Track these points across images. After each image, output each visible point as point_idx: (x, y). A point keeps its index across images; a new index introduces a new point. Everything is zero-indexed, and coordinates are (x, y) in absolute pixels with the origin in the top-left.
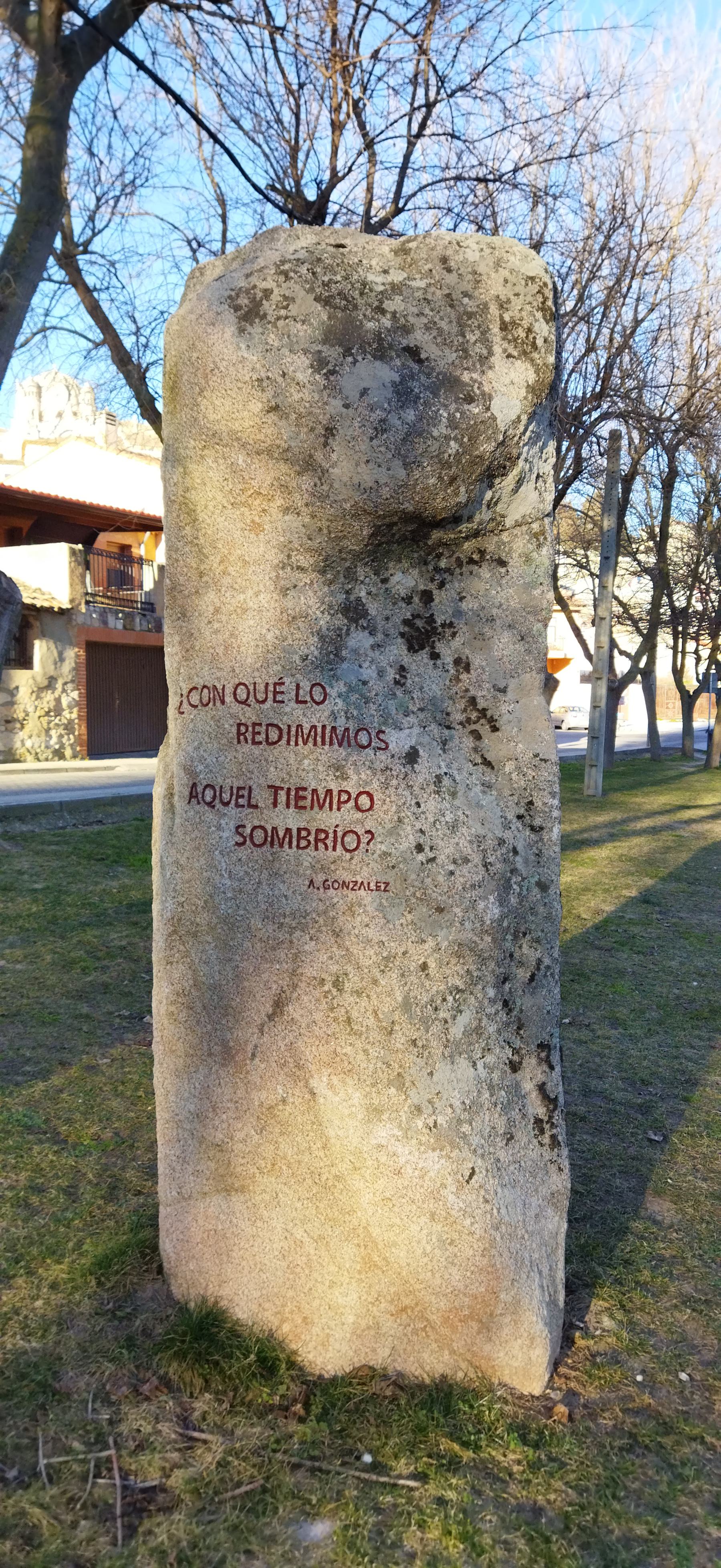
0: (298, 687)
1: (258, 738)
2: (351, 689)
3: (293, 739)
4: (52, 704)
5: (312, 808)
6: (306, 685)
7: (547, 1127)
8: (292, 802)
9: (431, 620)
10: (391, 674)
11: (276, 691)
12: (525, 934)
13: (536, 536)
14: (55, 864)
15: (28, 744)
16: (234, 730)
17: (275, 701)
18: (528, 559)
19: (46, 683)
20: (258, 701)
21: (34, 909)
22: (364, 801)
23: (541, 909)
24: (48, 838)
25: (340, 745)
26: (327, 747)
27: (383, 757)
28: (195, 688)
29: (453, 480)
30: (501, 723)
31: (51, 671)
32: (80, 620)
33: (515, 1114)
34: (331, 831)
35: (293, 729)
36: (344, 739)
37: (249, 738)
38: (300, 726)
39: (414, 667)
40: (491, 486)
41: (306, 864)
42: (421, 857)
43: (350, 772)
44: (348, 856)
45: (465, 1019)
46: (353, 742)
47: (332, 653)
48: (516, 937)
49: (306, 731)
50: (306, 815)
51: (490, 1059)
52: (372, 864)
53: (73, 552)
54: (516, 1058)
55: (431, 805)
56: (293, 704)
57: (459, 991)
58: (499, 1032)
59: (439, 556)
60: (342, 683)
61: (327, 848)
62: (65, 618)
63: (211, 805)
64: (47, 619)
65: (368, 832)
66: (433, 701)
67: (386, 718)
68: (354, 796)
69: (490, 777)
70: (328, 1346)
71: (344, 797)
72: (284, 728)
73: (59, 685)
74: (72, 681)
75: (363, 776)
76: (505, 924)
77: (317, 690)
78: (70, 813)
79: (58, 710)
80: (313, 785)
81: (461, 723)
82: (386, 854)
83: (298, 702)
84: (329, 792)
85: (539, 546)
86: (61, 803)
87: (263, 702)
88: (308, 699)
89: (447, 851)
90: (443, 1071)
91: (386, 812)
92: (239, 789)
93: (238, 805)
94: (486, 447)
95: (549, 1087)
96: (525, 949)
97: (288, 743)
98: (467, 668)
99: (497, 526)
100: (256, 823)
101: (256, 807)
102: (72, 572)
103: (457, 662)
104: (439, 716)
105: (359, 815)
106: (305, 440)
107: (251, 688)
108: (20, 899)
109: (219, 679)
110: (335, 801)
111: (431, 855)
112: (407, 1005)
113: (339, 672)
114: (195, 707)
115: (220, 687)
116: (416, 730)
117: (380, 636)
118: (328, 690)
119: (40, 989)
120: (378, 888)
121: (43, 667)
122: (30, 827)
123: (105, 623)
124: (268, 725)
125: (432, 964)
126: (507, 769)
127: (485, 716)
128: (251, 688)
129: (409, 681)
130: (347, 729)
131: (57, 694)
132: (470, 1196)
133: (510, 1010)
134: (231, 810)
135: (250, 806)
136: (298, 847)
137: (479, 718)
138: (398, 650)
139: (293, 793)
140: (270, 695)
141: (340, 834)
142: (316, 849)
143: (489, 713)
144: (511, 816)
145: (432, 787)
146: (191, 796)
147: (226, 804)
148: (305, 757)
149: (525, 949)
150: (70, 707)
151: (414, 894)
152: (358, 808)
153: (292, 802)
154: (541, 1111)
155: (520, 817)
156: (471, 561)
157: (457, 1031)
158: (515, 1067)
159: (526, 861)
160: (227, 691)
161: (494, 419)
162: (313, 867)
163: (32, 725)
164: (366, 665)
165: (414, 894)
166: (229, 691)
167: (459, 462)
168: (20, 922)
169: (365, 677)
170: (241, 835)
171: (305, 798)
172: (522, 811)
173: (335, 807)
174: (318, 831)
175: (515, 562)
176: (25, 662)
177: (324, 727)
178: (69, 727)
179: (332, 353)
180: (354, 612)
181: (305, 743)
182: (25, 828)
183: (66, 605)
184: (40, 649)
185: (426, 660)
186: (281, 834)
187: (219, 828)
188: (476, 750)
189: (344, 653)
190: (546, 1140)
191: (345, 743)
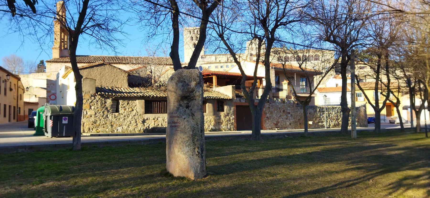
15: (223, 127)
31: (228, 112)
32: (235, 101)
36: (178, 117)
47: (178, 109)
53: (233, 87)
55: (186, 123)
70: (176, 174)
73: (230, 115)
79: (230, 120)
90: (185, 148)
94: (190, 90)
99: (195, 96)
102: (233, 91)
106: (175, 90)
112: (182, 142)
123: (241, 101)
132: (187, 159)
138: (185, 109)
150: (232, 119)
157: (187, 144)
158: (194, 149)
163: (224, 123)
176: (223, 110)
178: (232, 124)
179: (177, 83)
180: (180, 105)
184: (226, 108)
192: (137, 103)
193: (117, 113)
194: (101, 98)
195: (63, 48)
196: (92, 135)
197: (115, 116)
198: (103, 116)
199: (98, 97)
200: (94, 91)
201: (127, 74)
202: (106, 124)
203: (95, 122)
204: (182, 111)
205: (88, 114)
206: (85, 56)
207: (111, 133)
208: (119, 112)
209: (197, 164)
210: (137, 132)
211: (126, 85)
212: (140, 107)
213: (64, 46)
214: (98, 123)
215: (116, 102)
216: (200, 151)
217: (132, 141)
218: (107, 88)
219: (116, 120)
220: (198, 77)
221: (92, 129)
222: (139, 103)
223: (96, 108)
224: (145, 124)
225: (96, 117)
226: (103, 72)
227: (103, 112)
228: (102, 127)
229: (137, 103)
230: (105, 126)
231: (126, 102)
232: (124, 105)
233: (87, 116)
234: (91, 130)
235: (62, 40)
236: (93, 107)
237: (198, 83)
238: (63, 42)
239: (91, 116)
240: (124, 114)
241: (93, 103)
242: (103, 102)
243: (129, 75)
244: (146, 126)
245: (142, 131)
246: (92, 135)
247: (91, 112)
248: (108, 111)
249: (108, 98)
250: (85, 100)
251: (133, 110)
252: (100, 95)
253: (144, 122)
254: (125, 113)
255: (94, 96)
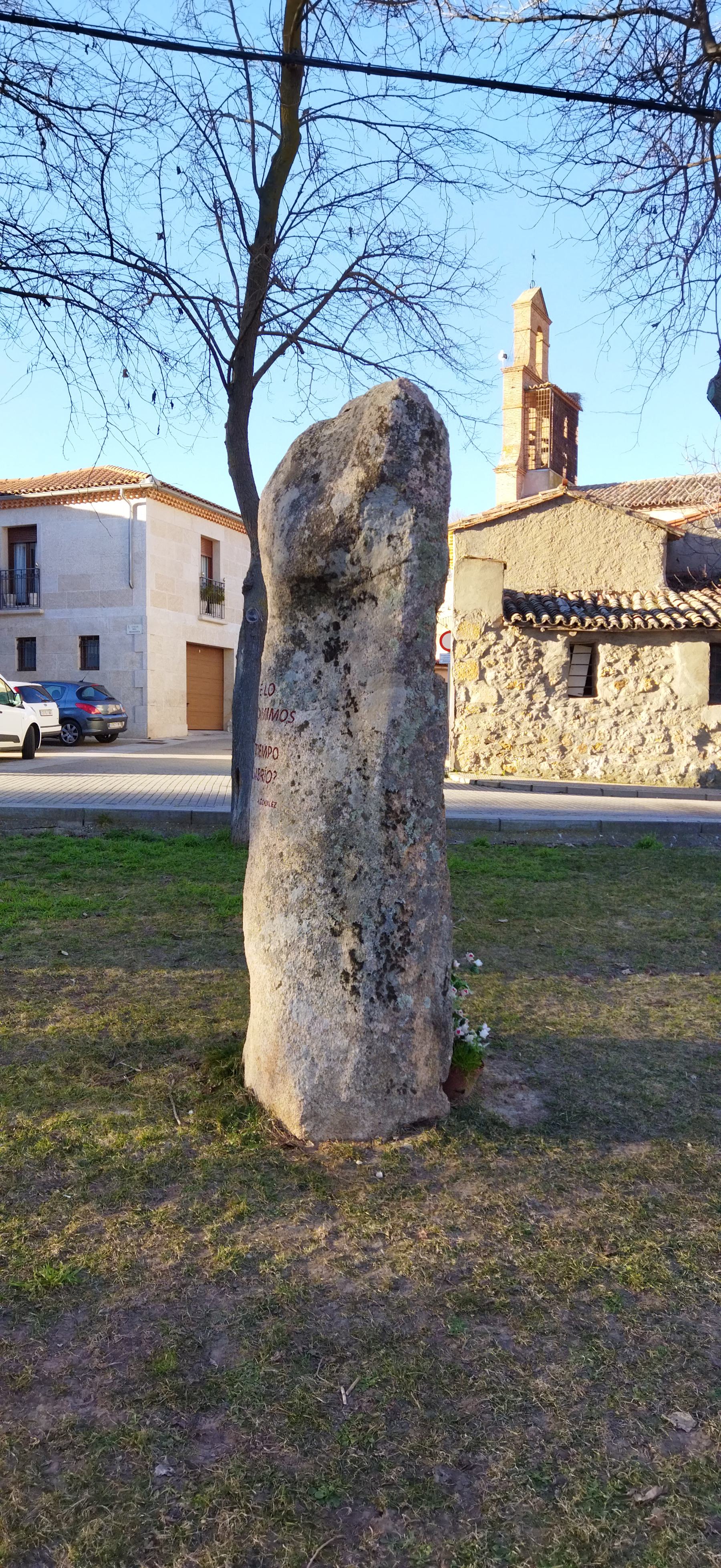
7: (351, 979)
9: (338, 639)
10: (313, 676)
12: (351, 847)
13: (394, 577)
18: (388, 594)
23: (363, 833)
29: (310, 553)
33: (326, 962)
40: (348, 551)
42: (292, 789)
45: (297, 892)
48: (344, 848)
51: (315, 922)
54: (337, 927)
57: (297, 873)
58: (326, 907)
59: (342, 599)
69: (349, 743)
76: (333, 837)
85: (396, 584)
90: (279, 919)
94: (328, 529)
95: (358, 953)
96: (352, 858)
99: (367, 575)
104: (333, 702)
117: (311, 653)
125: (285, 854)
133: (338, 896)
138: (320, 660)
144: (353, 768)
149: (352, 858)
154: (349, 968)
155: (359, 769)
156: (360, 600)
158: (335, 933)
159: (356, 799)
161: (331, 510)
167: (311, 542)
175: (381, 597)
189: (290, 665)
190: (349, 988)
192: (677, 658)
193: (588, 700)
194: (524, 638)
195: (532, 465)
196: (476, 784)
197: (577, 709)
198: (529, 709)
199: (510, 634)
200: (497, 610)
201: (662, 533)
202: (539, 741)
203: (497, 734)
204: (300, 676)
205: (474, 699)
206: (605, 486)
207: (557, 779)
208: (595, 695)
209: (341, 1041)
210: (671, 783)
211: (656, 579)
212: (686, 674)
213: (537, 459)
214: (509, 736)
215: (583, 648)
216: (367, 952)
217: (511, 823)
218: (571, 597)
219: (582, 726)
220: (383, 429)
221: (487, 759)
222: (684, 655)
223: (501, 678)
224: (710, 748)
225: (503, 712)
226: (563, 533)
227: (530, 694)
228: (525, 753)
229: (677, 658)
230: (534, 748)
231: (625, 652)
232: (619, 666)
233: (470, 706)
234: (483, 763)
235: (531, 437)
236: (489, 675)
237: (382, 479)
238: (532, 443)
239: (484, 710)
240: (614, 704)
241: (490, 658)
242: (531, 652)
243: (670, 538)
244: (710, 759)
245: (692, 779)
246: (476, 784)
247: (483, 694)
248: (550, 691)
249: (551, 635)
250: (464, 645)
251: (655, 688)
252: (516, 623)
253: (703, 738)
254: (621, 700)
255: (498, 629)
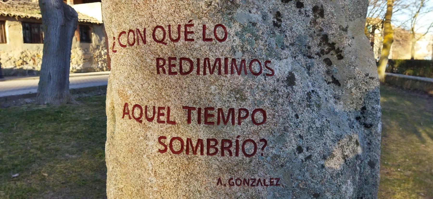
0: (204, 27)
1: (174, 70)
2: (244, 29)
3: (202, 70)
4: (98, 54)
5: (218, 123)
6: (210, 26)
8: (203, 119)
10: (271, 18)
11: (187, 30)
14: (95, 109)
16: (154, 63)
17: (186, 39)
19: (96, 47)
20: (172, 40)
21: (84, 129)
22: (259, 116)
24: (94, 99)
25: (239, 73)
26: (229, 75)
27: (271, 82)
28: (124, 32)
30: (345, 53)
31: (97, 43)
34: (234, 141)
35: (202, 62)
37: (167, 69)
38: (207, 59)
39: (285, 13)
41: (214, 166)
42: (301, 156)
43: (248, 94)
44: (248, 159)
46: (248, 70)
49: (212, 63)
50: (214, 129)
52: (267, 165)
56: (201, 42)
60: (237, 25)
61: (231, 154)
62: (101, 26)
63: (139, 120)
64: (95, 27)
65: (263, 140)
66: (299, 38)
67: (270, 51)
68: (251, 112)
71: (243, 114)
72: (195, 61)
74: (105, 47)
75: (257, 97)
77: (220, 30)
78: (102, 90)
80: (219, 106)
81: (317, 54)
82: (276, 156)
83: (205, 39)
84: (232, 110)
86: (99, 86)
87: (177, 40)
88: (213, 37)
89: (318, 149)
91: (275, 124)
92: (160, 108)
93: (159, 121)
97: (198, 72)
98: (322, 14)
100: (175, 135)
101: (174, 123)
103: (315, 9)
104: (304, 49)
105: (255, 127)
107: (167, 29)
108: (80, 125)
109: (141, 24)
110: (236, 117)
111: (308, 154)
113: (235, 15)
114: (124, 46)
115: (141, 30)
116: (290, 60)
118: (228, 30)
119: (81, 167)
120: (272, 183)
121: (95, 42)
122: (88, 95)
124: (181, 59)
126: (349, 86)
127: (333, 48)
128: (167, 29)
129: (283, 24)
130: (243, 61)
131: (100, 51)
134: (154, 124)
135: (169, 122)
136: (208, 153)
137: (330, 50)
139: (203, 112)
140: (182, 35)
141: (241, 143)
142: (223, 155)
143: (336, 46)
145: (306, 102)
146: (124, 113)
147: (150, 120)
148: (212, 83)
150: (104, 55)
151: (298, 186)
152: (254, 122)
153: (203, 119)
160: (147, 33)
162: (220, 169)
164: (254, 11)
165: (298, 186)
166: (149, 32)
168: (78, 135)
169: (253, 20)
170: (163, 144)
171: (212, 116)
172: (359, 114)
173: (236, 122)
174: (224, 141)
177: (226, 59)
181: (212, 72)
182: (86, 95)
183: (101, 22)
185: (294, 8)
186: (194, 144)
187: (146, 138)
188: (328, 72)
191: (243, 72)
